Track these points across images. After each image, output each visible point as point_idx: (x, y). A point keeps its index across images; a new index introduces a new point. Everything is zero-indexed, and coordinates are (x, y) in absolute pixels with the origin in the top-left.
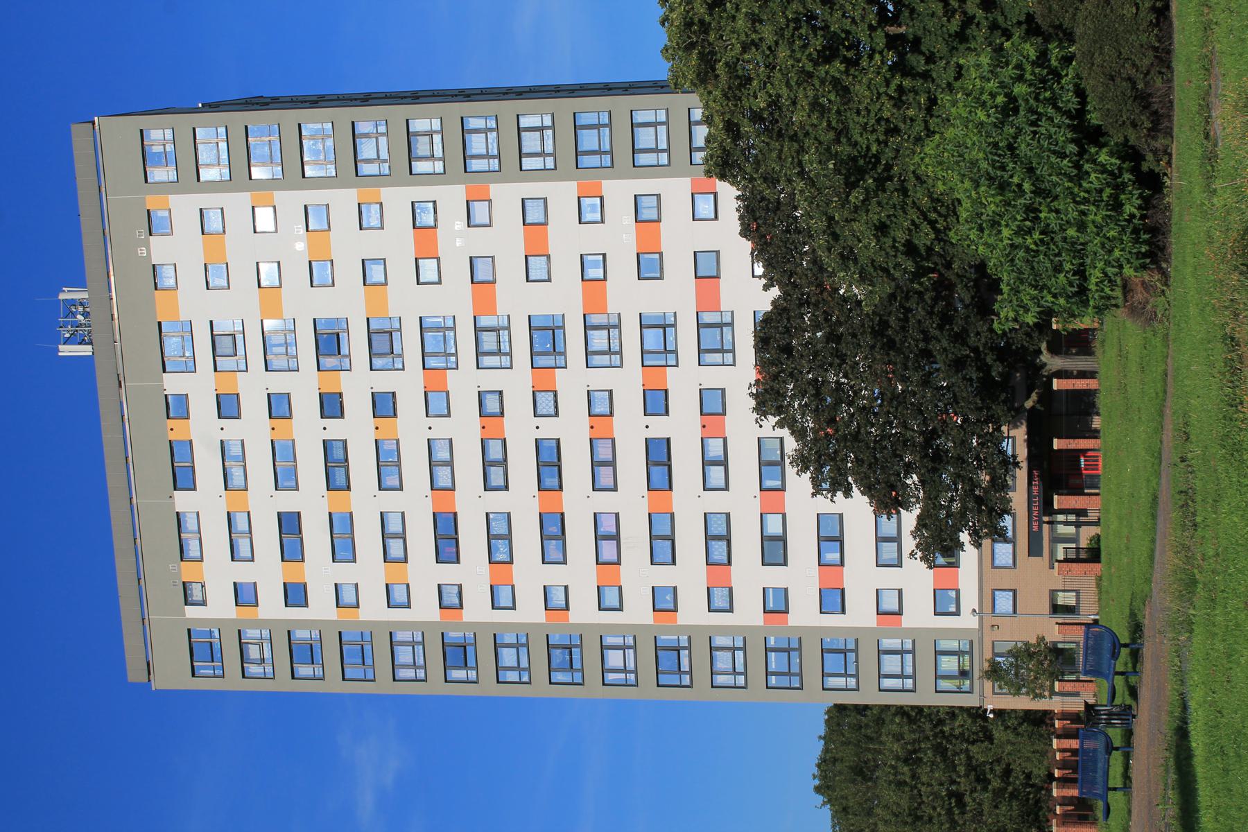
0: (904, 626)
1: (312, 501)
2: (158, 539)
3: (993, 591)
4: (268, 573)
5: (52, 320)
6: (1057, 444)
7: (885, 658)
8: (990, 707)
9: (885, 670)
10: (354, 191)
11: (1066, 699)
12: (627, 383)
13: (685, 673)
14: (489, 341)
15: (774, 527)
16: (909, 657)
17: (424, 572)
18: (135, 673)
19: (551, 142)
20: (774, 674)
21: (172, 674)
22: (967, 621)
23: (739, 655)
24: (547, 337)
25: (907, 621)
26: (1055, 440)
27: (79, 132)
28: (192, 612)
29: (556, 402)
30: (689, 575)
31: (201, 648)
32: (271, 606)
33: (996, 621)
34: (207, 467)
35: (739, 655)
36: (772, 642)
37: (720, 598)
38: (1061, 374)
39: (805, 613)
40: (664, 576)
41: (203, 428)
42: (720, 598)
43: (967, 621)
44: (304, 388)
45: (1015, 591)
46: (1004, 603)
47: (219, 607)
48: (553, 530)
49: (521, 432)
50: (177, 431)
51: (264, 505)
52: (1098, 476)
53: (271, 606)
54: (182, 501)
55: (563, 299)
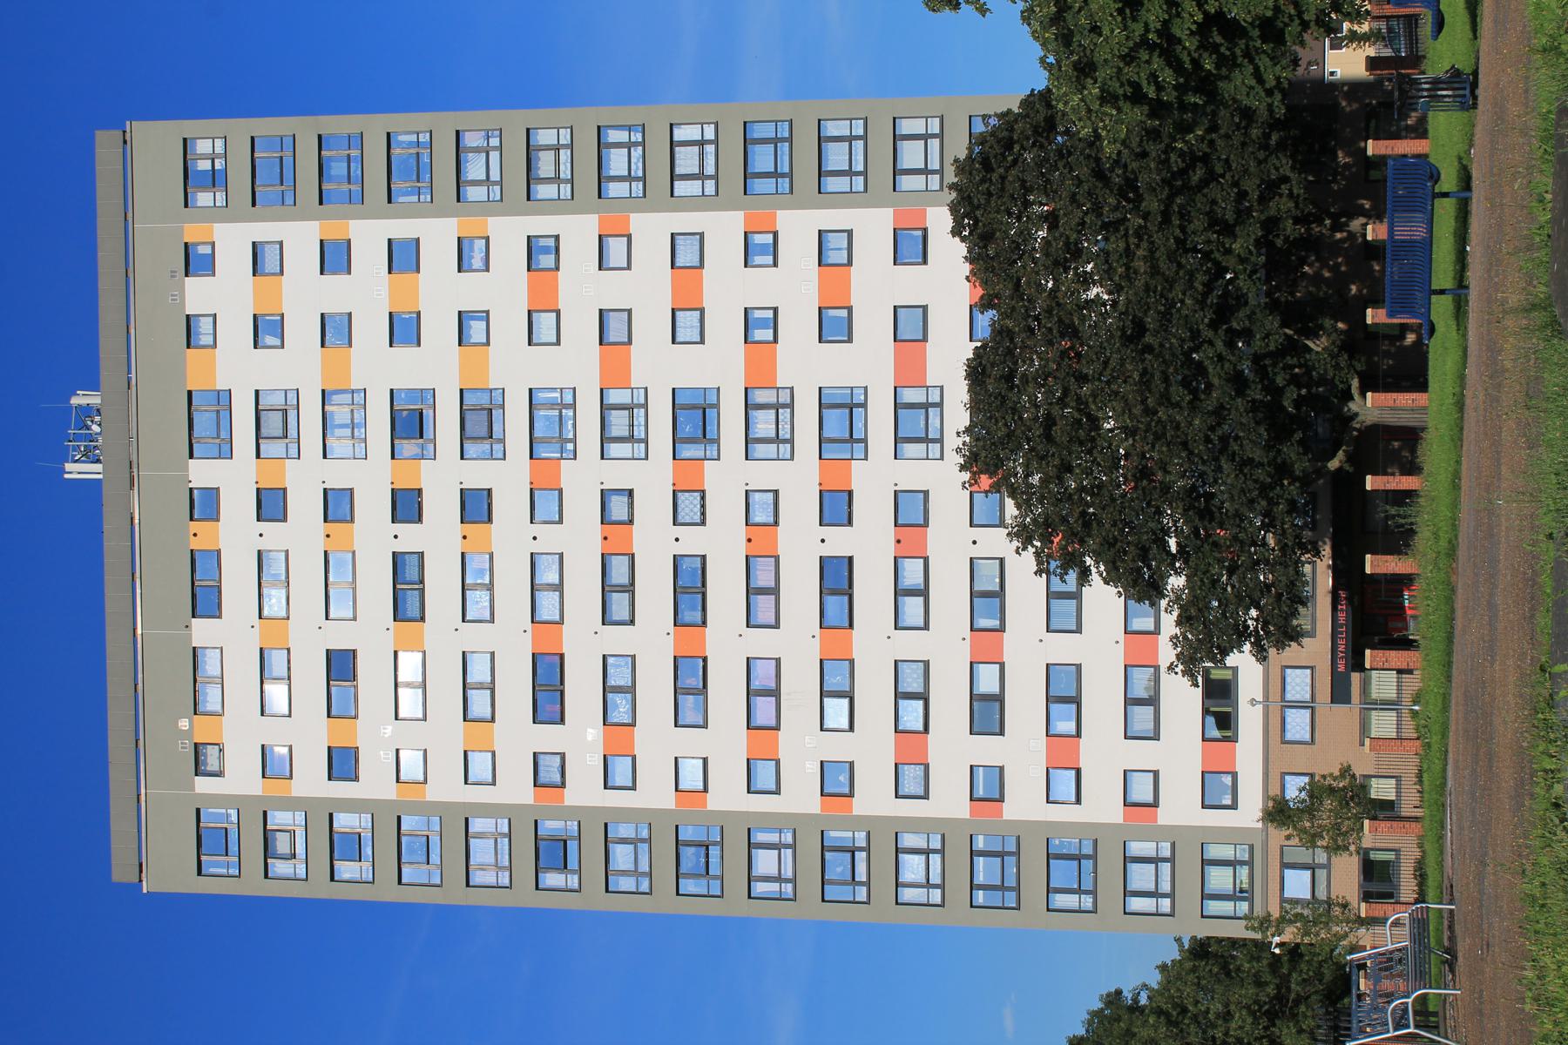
7: (1134, 868)
13: (861, 884)
15: (988, 681)
18: (121, 871)
21: (168, 869)
24: (695, 418)
25: (714, 802)
27: (106, 143)
28: (203, 785)
29: (703, 506)
35: (935, 859)
47: (241, 777)
50: (202, 536)
53: (311, 780)
54: (202, 631)
55: (719, 366)
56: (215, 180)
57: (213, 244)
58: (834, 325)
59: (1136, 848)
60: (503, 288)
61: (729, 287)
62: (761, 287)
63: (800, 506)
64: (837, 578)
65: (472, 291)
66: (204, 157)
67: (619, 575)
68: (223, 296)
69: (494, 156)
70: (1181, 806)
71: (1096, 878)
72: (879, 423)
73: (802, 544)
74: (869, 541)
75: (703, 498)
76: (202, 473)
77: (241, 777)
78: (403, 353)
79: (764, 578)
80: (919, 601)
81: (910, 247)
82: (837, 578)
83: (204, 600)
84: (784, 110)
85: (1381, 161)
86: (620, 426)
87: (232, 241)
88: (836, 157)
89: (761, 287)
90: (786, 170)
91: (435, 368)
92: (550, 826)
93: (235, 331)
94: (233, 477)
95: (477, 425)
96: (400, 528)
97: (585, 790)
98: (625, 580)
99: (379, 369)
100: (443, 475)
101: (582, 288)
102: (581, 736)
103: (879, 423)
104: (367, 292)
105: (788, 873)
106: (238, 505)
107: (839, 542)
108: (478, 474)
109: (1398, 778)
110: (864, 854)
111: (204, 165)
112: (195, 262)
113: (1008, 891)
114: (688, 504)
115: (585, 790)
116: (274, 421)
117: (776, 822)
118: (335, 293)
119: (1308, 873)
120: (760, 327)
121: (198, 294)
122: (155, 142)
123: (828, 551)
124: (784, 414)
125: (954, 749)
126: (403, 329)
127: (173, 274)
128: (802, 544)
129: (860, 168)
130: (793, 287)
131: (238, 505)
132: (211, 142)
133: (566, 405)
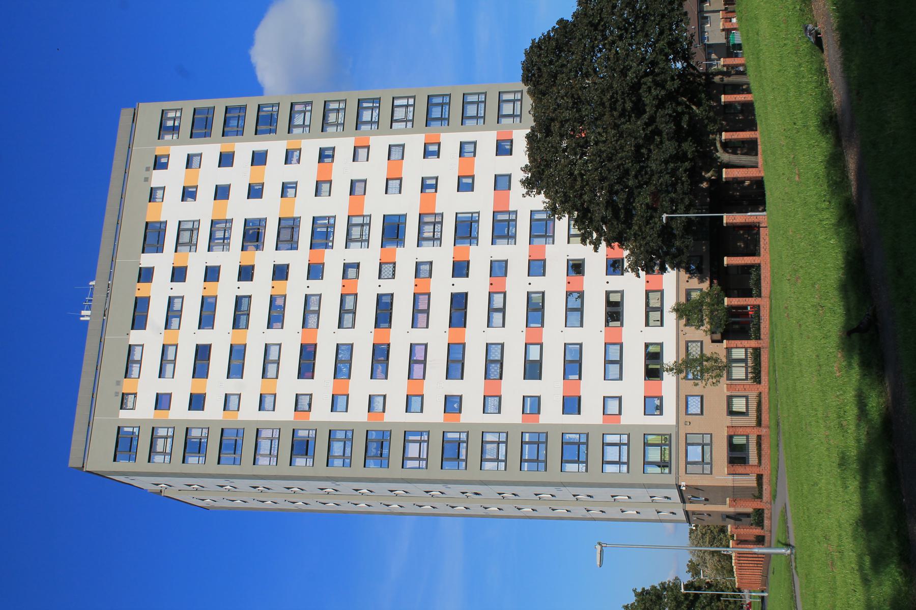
0: (622, 423)
1: (220, 338)
2: (113, 361)
3: (687, 397)
4: (181, 385)
5: (82, 299)
6: (726, 260)
7: (608, 448)
8: (683, 484)
9: (608, 459)
10: (286, 142)
11: (737, 477)
12: (443, 256)
13: (463, 460)
14: (356, 232)
15: (534, 355)
16: (625, 448)
17: (288, 383)
18: (74, 461)
19: (411, 114)
20: (526, 461)
21: (99, 457)
22: (668, 418)
23: (502, 447)
24: (393, 230)
25: (625, 420)
26: (725, 258)
27: (126, 115)
28: (124, 414)
29: (394, 271)
30: (472, 386)
31: (125, 444)
32: (179, 410)
33: (689, 418)
34: (157, 313)
35: (502, 447)
36: (527, 438)
37: (492, 400)
38: (729, 166)
39: (552, 414)
40: (454, 387)
41: (159, 291)
42: (492, 400)
43: (668, 418)
44: (229, 260)
45: (702, 397)
46: (694, 407)
47: (143, 410)
48: (381, 355)
49: (368, 289)
50: (142, 290)
51: (189, 334)
52: (758, 267)
53: (179, 410)
54: (136, 337)
55: (408, 204)
56: (175, 129)
57: (439, 144)
58: (465, 184)
59: (609, 439)
60: (306, 172)
61: (415, 167)
62: (431, 167)
63: (369, 270)
64: (459, 302)
65: (290, 173)
66: (170, 119)
67: (349, 305)
68: (171, 179)
69: (308, 114)
70: (633, 414)
71: (587, 454)
72: (485, 229)
73: (443, 286)
74: (476, 286)
75: (394, 267)
76: (147, 260)
77: (143, 410)
78: (254, 201)
79: (654, 303)
80: (500, 315)
81: (504, 148)
82: (459, 302)
83: (139, 321)
84: (341, 95)
85: (729, 105)
86: (356, 234)
87: (177, 153)
88: (399, 114)
89: (431, 167)
90: (411, 118)
91: (269, 209)
92: (302, 434)
93: (174, 193)
94: (161, 263)
95: (286, 235)
96: (611, 278)
97: (321, 413)
98: (501, 306)
99: (240, 209)
100: (265, 259)
101: (343, 170)
102: (251, 383)
103: (485, 229)
104: (239, 176)
105: (624, 459)
106: (162, 275)
107: (538, 284)
108: (283, 257)
109: (747, 397)
110: (465, 445)
111: (170, 123)
112: (159, 164)
113: (539, 462)
114: (387, 269)
115: (321, 413)
116: (187, 235)
117: (270, 425)
118: (224, 176)
119: (700, 448)
120: (428, 186)
121: (158, 178)
122: (149, 113)
123: (382, 291)
124: (366, 228)
125: (436, 385)
126: (255, 192)
127: (148, 169)
128: (443, 286)
129: (411, 118)
130: (446, 168)
131: (162, 275)
132: (184, 110)
133: (194, 230)
